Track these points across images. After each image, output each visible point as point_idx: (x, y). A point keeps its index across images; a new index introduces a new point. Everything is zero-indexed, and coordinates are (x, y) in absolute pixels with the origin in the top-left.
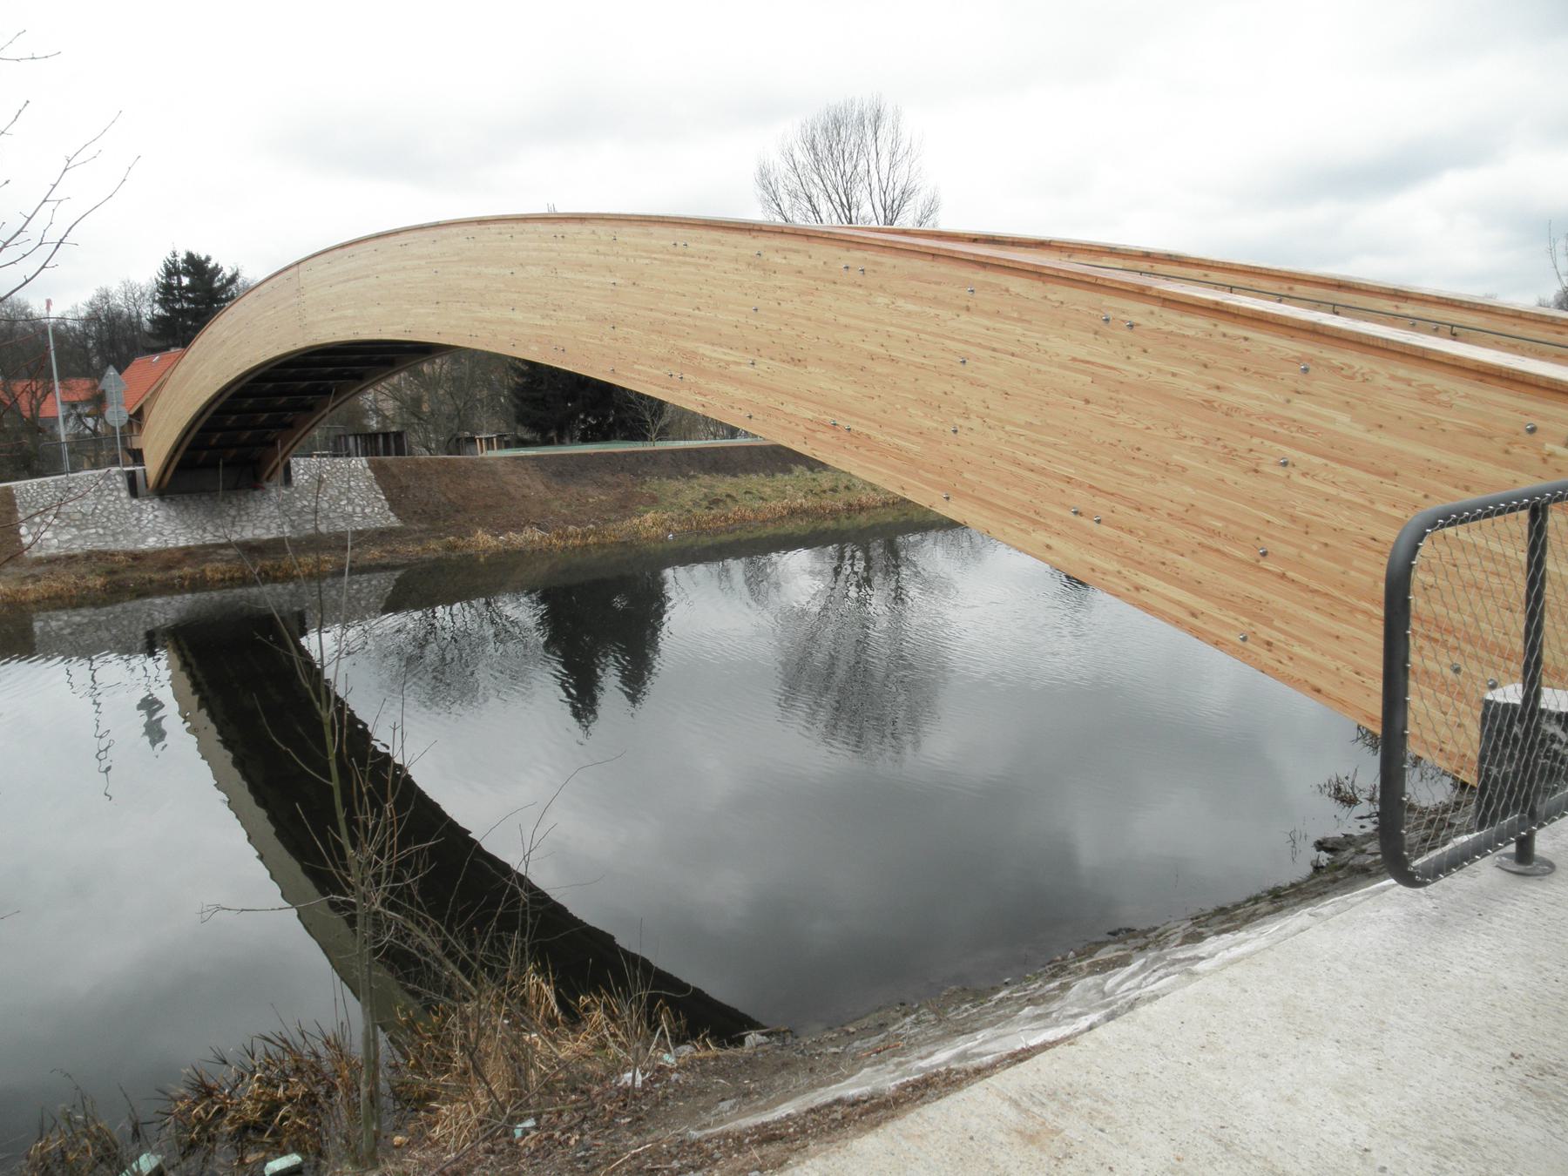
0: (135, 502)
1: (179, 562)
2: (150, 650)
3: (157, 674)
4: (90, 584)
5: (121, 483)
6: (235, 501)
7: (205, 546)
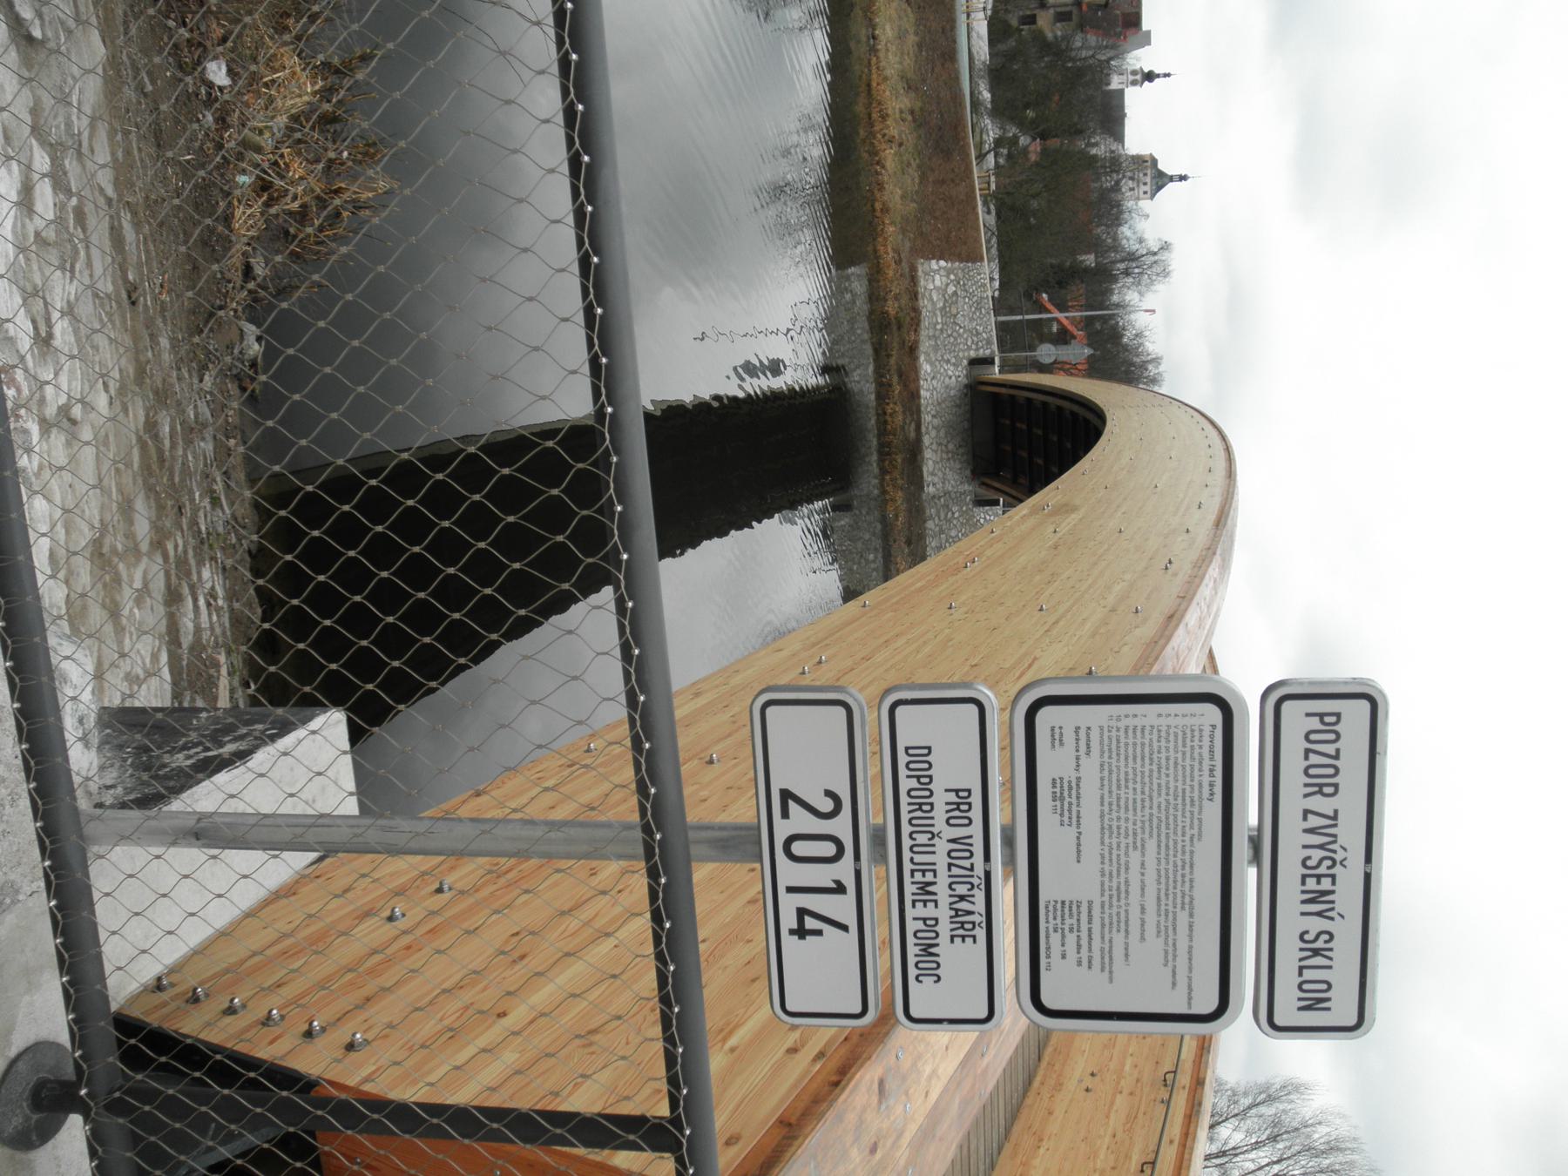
0: (965, 362)
1: (905, 386)
2: (825, 369)
3: (800, 368)
4: (890, 303)
5: (984, 353)
6: (961, 451)
7: (919, 411)
